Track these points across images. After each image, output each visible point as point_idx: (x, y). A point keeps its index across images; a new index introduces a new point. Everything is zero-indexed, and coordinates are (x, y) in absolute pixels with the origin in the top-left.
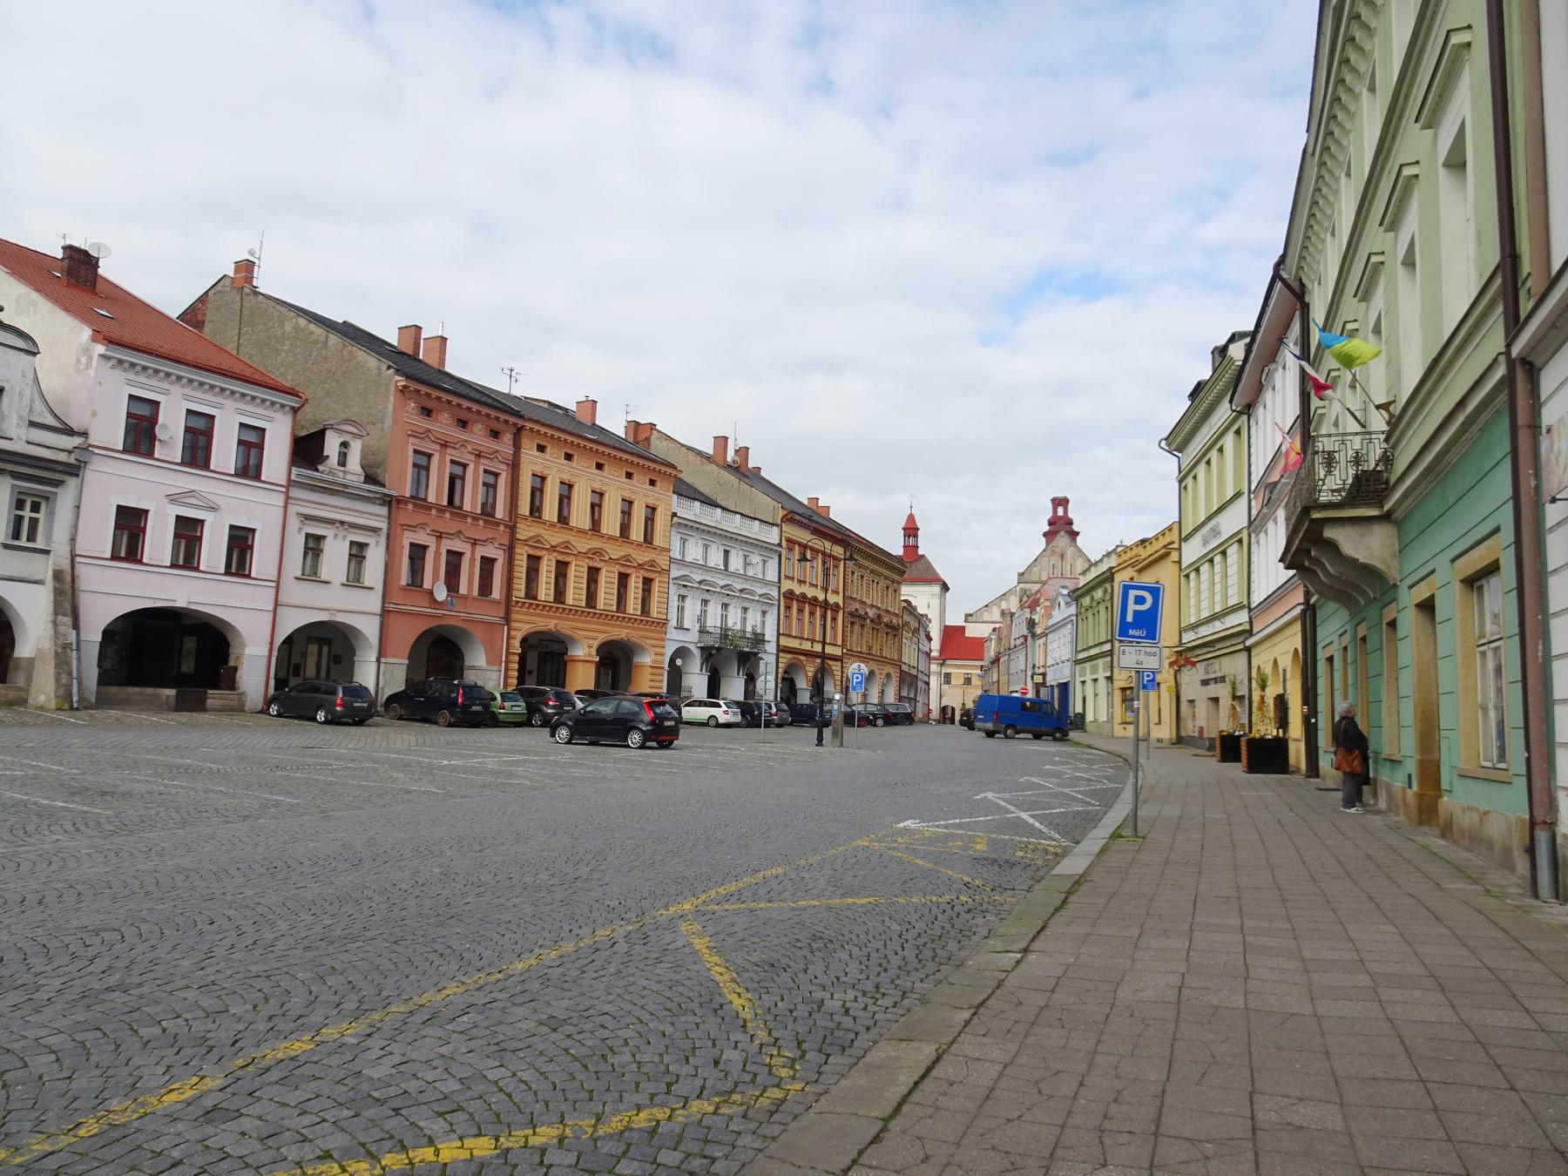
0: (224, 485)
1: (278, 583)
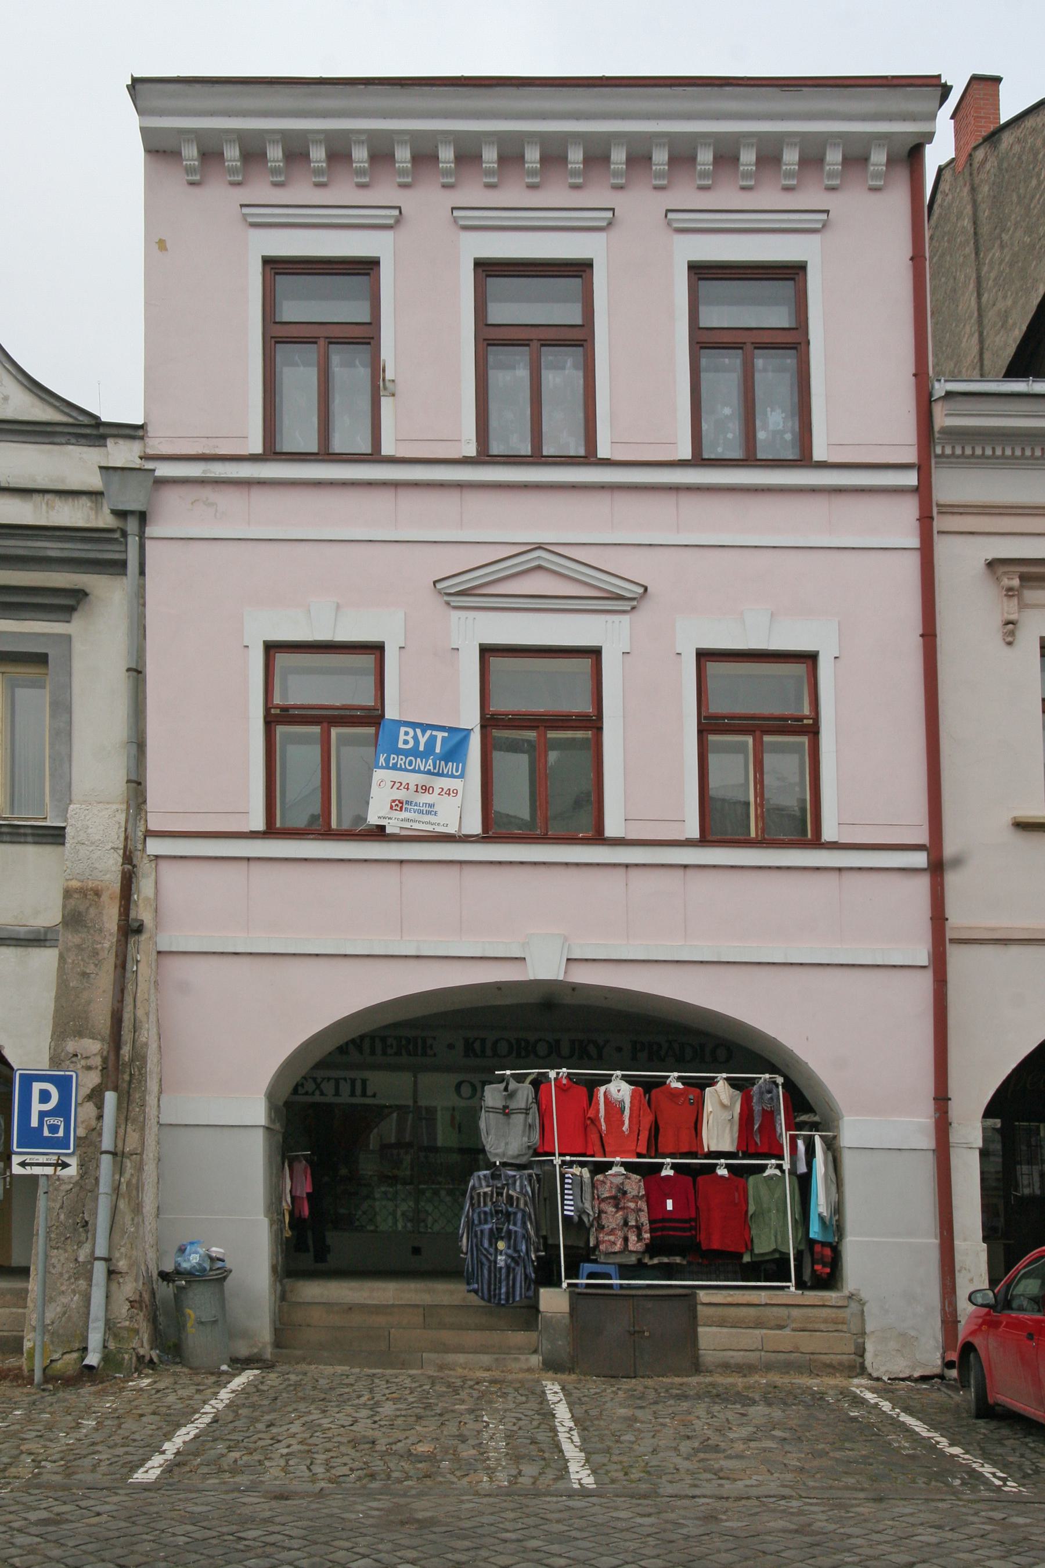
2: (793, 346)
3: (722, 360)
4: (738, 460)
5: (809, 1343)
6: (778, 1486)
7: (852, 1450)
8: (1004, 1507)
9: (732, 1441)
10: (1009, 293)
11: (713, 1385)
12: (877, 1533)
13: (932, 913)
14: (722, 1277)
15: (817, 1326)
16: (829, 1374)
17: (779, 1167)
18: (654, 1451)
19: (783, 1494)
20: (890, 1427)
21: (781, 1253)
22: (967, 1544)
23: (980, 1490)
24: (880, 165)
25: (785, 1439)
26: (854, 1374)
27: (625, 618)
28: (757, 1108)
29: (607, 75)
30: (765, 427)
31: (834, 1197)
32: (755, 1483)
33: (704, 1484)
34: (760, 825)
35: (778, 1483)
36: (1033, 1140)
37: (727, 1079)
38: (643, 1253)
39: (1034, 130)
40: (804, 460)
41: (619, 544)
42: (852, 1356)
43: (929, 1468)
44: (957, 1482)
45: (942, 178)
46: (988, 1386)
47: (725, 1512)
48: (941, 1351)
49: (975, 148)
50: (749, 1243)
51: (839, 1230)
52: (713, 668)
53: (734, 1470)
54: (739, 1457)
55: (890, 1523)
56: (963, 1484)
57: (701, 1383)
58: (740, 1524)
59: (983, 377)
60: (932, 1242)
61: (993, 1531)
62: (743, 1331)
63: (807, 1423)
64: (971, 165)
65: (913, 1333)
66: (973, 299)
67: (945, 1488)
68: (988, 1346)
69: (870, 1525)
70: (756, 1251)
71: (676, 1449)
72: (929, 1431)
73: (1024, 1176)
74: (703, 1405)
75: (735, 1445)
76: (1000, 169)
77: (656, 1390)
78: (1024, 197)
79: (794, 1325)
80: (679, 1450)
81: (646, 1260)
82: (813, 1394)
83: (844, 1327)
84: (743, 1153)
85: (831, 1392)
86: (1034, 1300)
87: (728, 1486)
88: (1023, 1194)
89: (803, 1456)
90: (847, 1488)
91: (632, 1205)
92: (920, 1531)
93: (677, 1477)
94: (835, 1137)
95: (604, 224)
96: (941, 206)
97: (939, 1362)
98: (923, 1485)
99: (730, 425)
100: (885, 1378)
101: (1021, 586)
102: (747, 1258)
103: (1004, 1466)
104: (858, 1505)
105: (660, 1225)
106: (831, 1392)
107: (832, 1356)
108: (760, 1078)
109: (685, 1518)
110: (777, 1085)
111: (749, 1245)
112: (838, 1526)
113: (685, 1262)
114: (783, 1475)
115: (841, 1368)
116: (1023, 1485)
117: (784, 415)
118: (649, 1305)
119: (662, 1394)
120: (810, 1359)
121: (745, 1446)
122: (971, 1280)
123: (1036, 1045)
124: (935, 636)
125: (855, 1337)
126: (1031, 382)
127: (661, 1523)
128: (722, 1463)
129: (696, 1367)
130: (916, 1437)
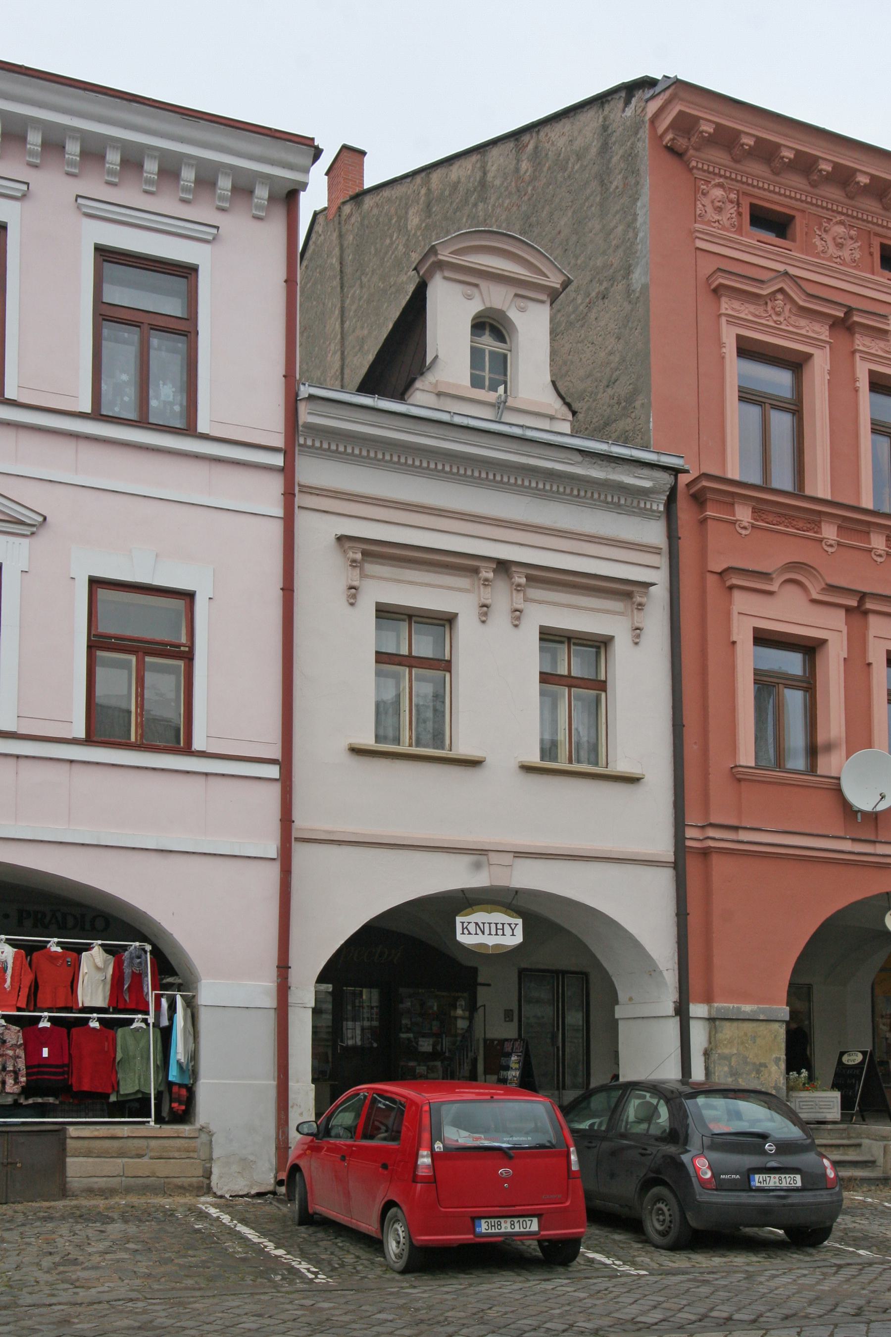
0: (66, 450)
1: (286, 763)
2: (184, 334)
3: (121, 333)
4: (132, 420)
5: (163, 1169)
6: (127, 1291)
7: (194, 1256)
8: (314, 1295)
9: (90, 1254)
10: (366, 325)
11: (77, 1207)
12: (208, 1324)
13: (282, 815)
14: (91, 1114)
15: (171, 1155)
16: (179, 1195)
17: (145, 1021)
18: (18, 1267)
19: (130, 1297)
20: (227, 1236)
21: (143, 1093)
22: (282, 1328)
23: (297, 1283)
24: (262, 199)
25: (137, 1251)
26: (200, 1194)
27: (25, 541)
28: (127, 971)
29: (26, 65)
30: (157, 398)
31: (191, 1046)
32: (107, 1289)
33: (62, 1293)
34: (140, 732)
35: (127, 1288)
36: (357, 1001)
37: (102, 945)
38: (19, 1094)
39: (389, 200)
40: (189, 429)
41: (22, 476)
42: (201, 1179)
43: (256, 1267)
44: (279, 1278)
45: (317, 221)
46: (309, 1199)
47: (77, 1316)
48: (274, 1172)
49: (344, 203)
50: (115, 1085)
51: (194, 1074)
52: (103, 594)
53: (89, 1279)
54: (95, 1268)
55: (220, 1315)
56: (283, 1279)
57: (66, 1206)
58: (90, 1325)
59: (343, 388)
60: (271, 1083)
61: (303, 1315)
62: (107, 1160)
63: (157, 1236)
64: (340, 216)
65: (251, 1158)
66: (337, 323)
67: (268, 1284)
68: (311, 1168)
69: (203, 1318)
70: (122, 1092)
71: (38, 1264)
72: (259, 1237)
73: (349, 1031)
74: (67, 1225)
75: (93, 1258)
76: (362, 224)
77: (25, 1214)
78: (380, 251)
79: (152, 1154)
80: (41, 1265)
81: (22, 1101)
82: (165, 1212)
83: (195, 1155)
84: (114, 1008)
85: (181, 1209)
86: (348, 1129)
87: (83, 1295)
88: (347, 1045)
89: (151, 1264)
90: (186, 1289)
91: (10, 1053)
92: (243, 1320)
93: (36, 1288)
94: (194, 997)
95: (19, 194)
96: (315, 243)
97: (272, 1181)
98: (251, 1282)
99: (127, 390)
100: (227, 1196)
101: (362, 559)
102: (113, 1098)
103: (317, 1262)
104: (195, 1302)
105: (35, 1070)
106: (181, 1209)
107: (184, 1179)
108: (131, 945)
109: (40, 1323)
110: (146, 952)
111: (116, 1087)
112: (176, 1320)
113: (57, 1102)
114: (132, 1281)
115: (191, 1189)
116: (330, 1277)
117: (174, 389)
118: (21, 1139)
119: (30, 1217)
120: (164, 1183)
121: (101, 1258)
122: (301, 1114)
123: (360, 926)
124: (293, 591)
125: (204, 1162)
126: (376, 399)
127: (17, 1330)
128: (79, 1273)
129: (64, 1192)
130: (248, 1243)
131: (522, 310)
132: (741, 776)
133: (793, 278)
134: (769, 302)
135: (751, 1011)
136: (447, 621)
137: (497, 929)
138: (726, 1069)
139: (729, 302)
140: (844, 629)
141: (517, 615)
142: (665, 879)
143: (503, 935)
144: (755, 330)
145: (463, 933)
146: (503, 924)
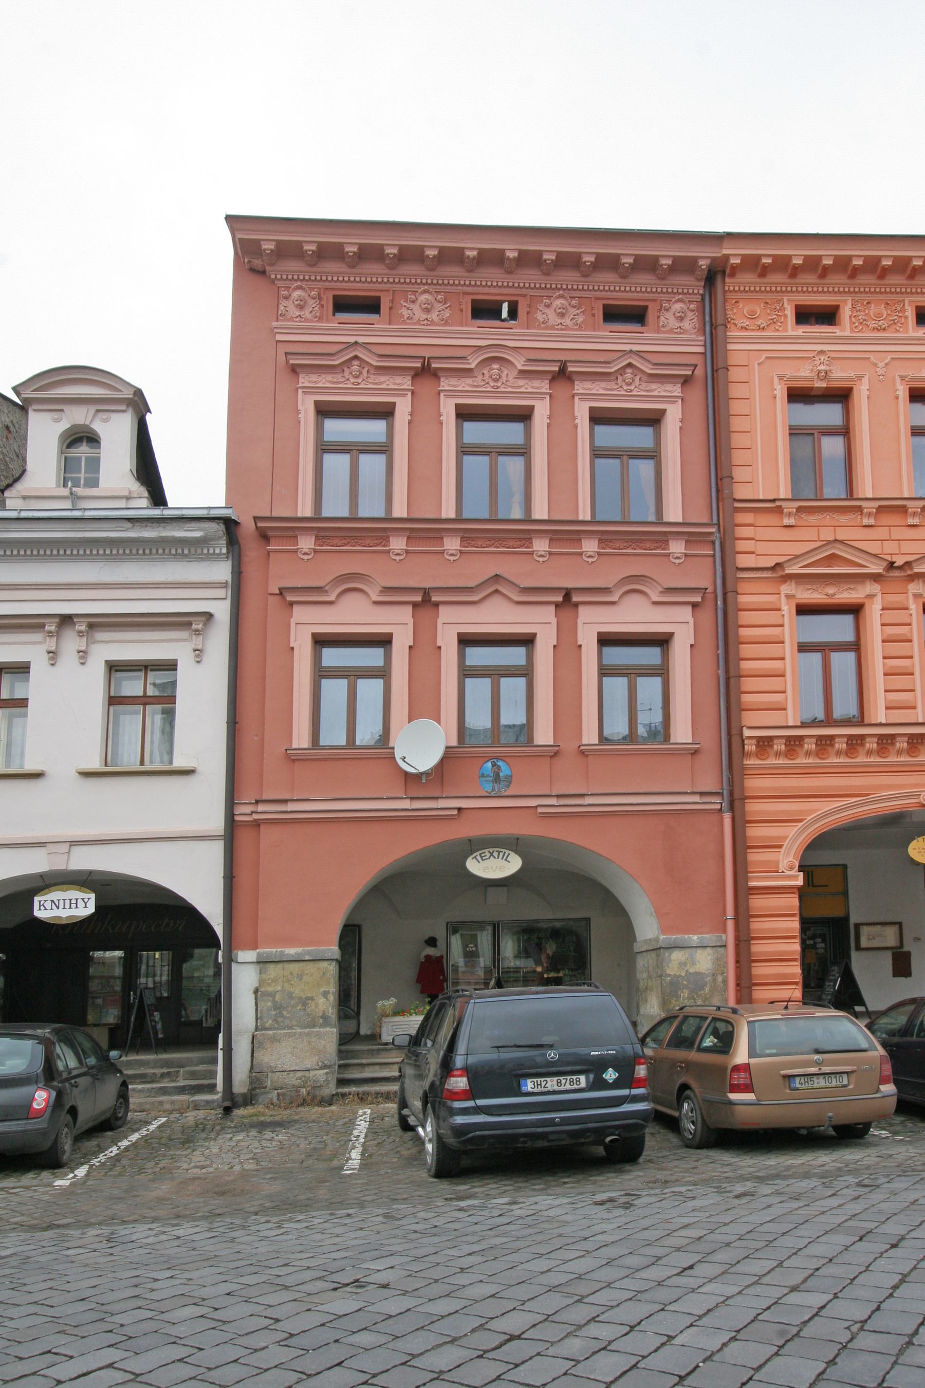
131: (106, 421)
132: (294, 757)
133: (638, 353)
134: (619, 377)
135: (296, 954)
136: (171, 666)
137: (71, 904)
138: (270, 1004)
139: (581, 385)
140: (691, 620)
141: (83, 655)
142: (217, 850)
143: (77, 907)
144: (636, 401)
145: (40, 909)
146: (77, 899)
